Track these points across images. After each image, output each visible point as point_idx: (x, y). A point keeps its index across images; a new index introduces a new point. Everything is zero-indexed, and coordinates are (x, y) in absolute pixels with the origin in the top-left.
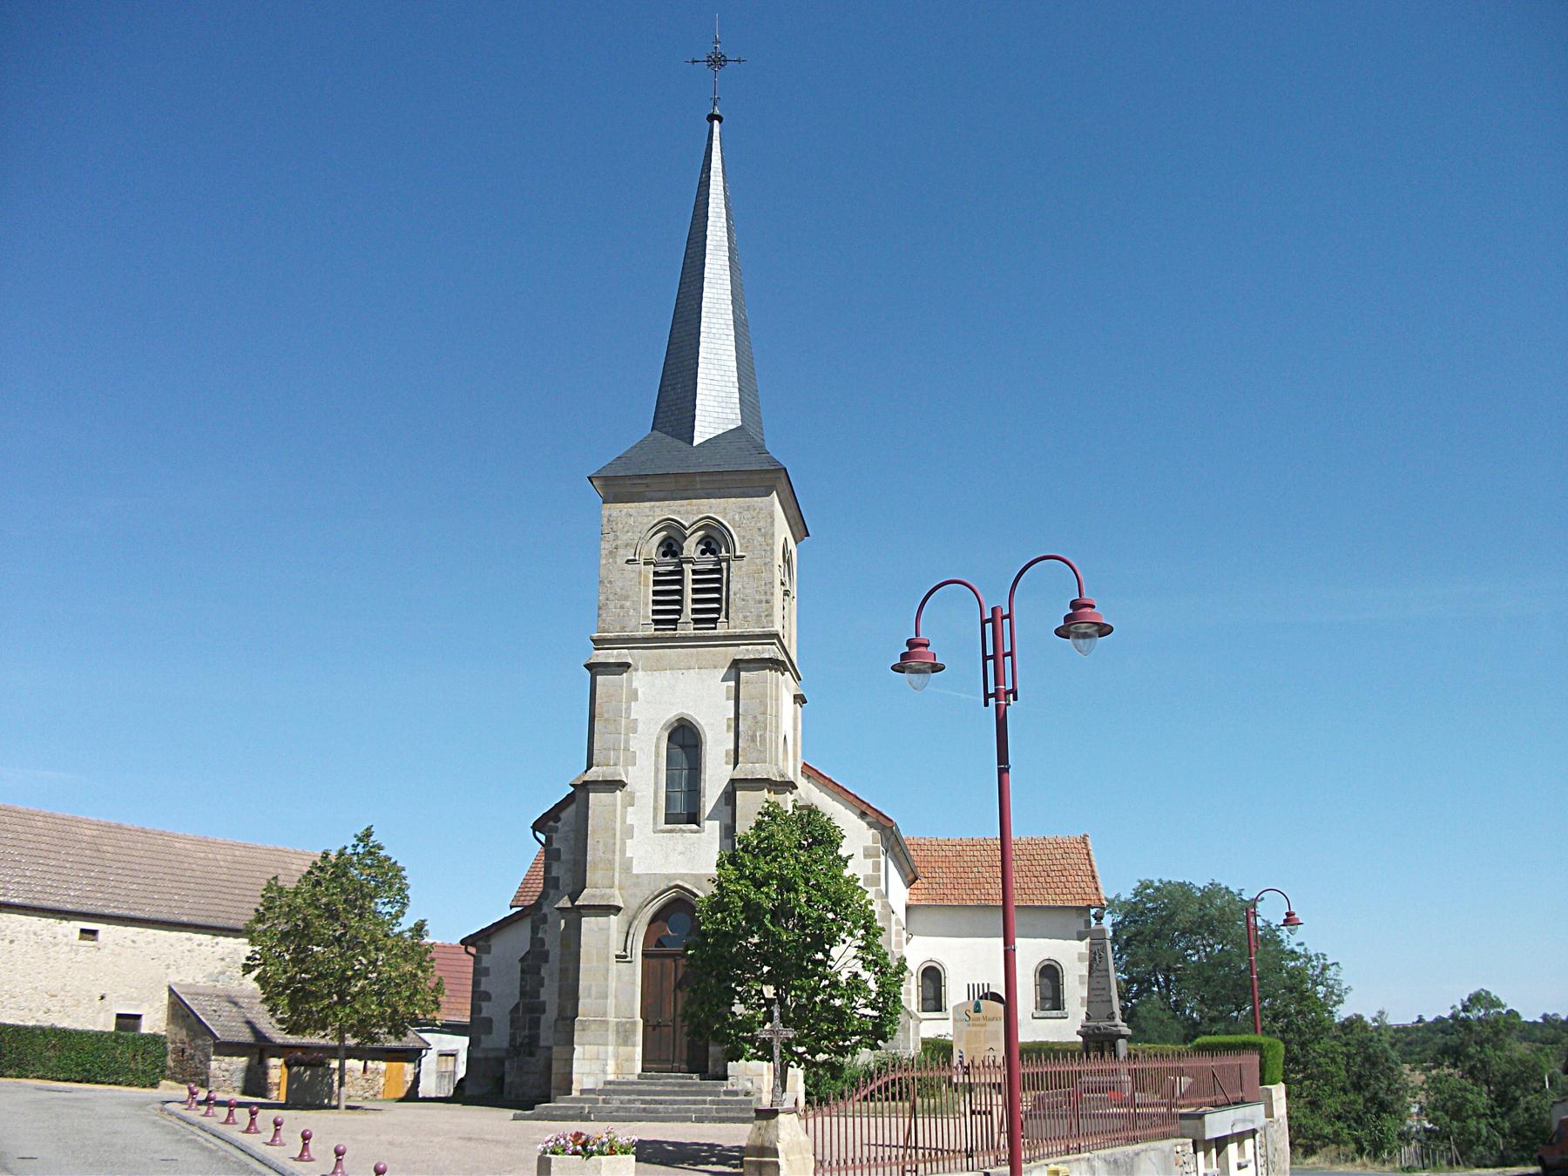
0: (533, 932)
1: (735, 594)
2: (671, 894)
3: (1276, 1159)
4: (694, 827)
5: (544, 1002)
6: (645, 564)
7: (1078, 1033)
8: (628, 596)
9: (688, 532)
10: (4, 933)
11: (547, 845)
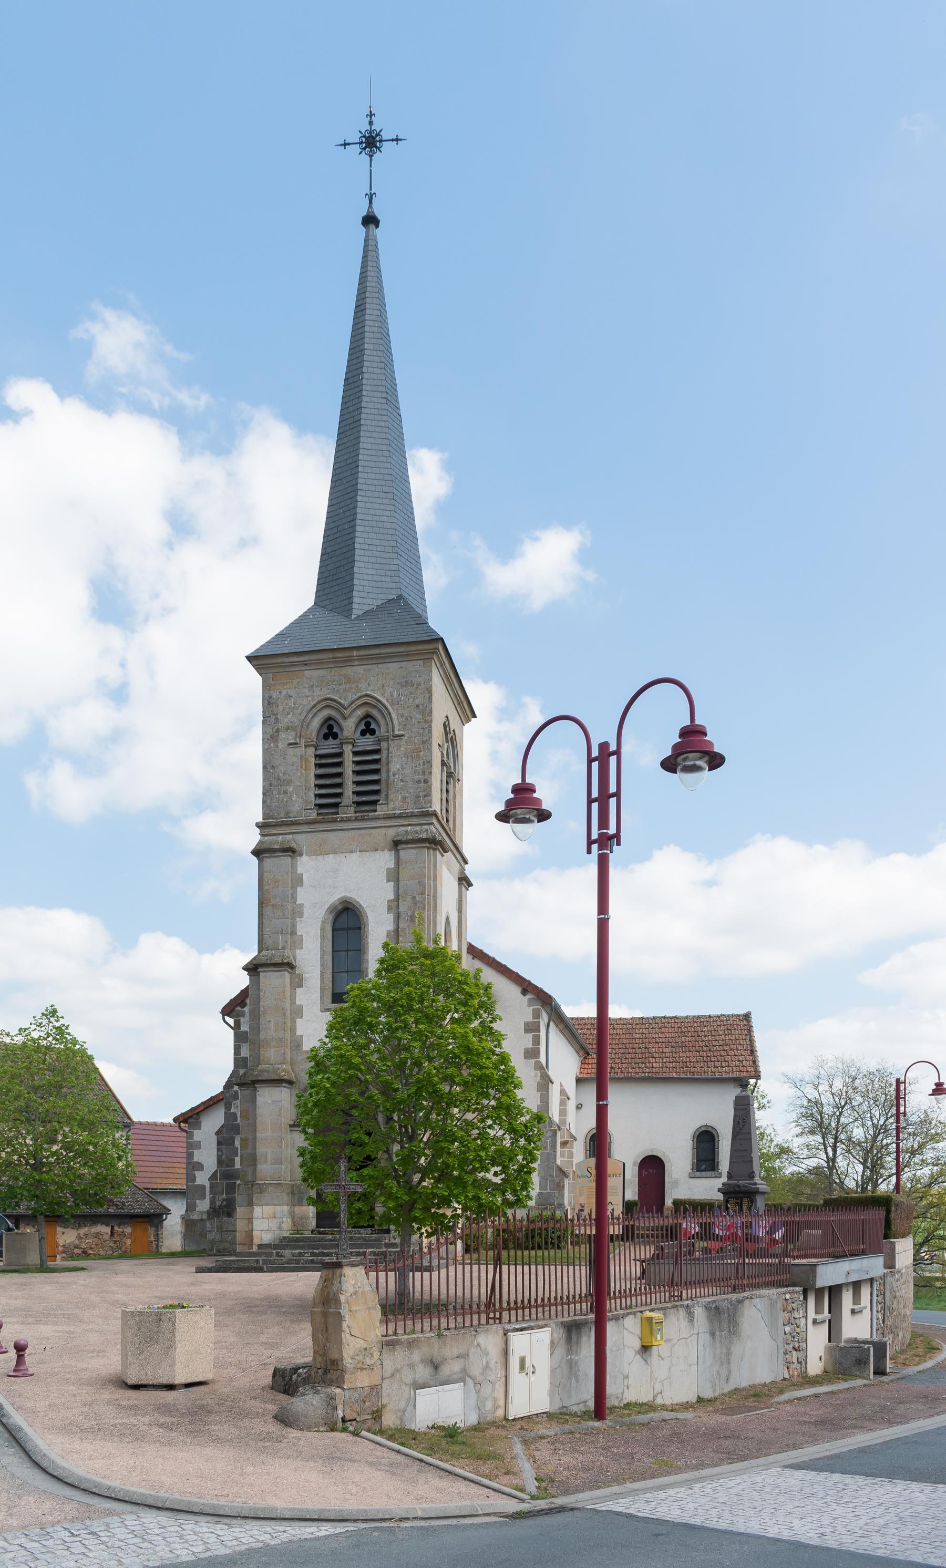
3: (895, 1306)
6: (306, 746)
7: (719, 1190)
8: (291, 781)
9: (347, 712)
11: (236, 1027)
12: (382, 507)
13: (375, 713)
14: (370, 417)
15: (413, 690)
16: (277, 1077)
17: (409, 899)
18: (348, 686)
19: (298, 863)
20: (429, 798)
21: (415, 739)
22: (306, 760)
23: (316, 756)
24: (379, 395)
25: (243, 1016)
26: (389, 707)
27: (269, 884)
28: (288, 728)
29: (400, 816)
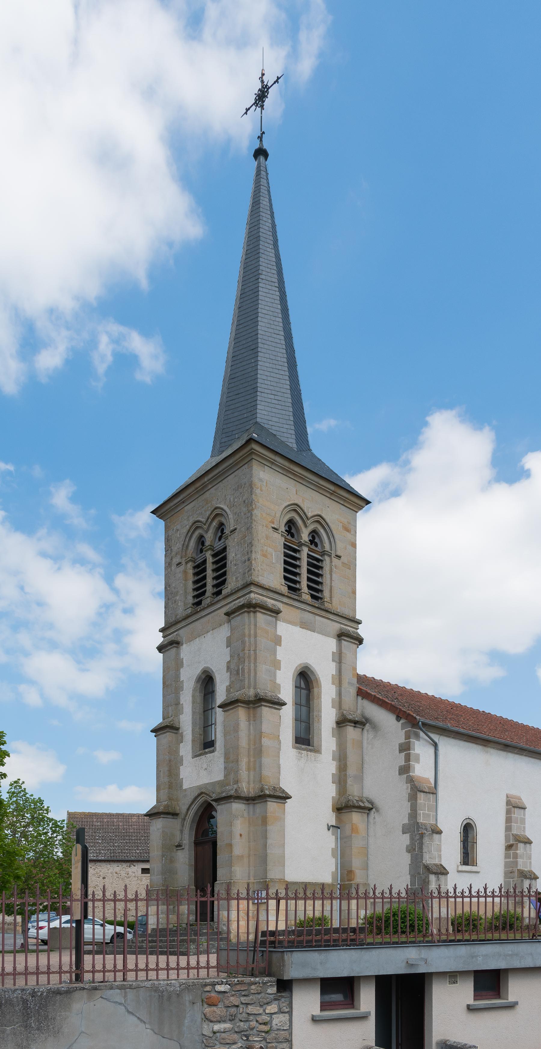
10: (99, 874)
13: (322, 531)
19: (181, 651)
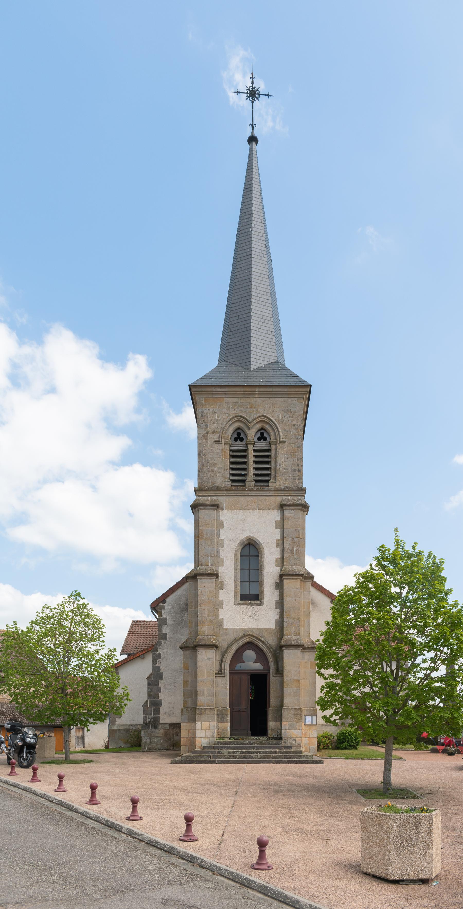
0: (153, 663)
1: (280, 465)
2: (245, 640)
4: (258, 602)
5: (161, 700)
6: (225, 444)
9: (251, 425)
12: (265, 307)
13: (267, 427)
14: (257, 254)
15: (291, 415)
16: (211, 644)
17: (290, 539)
18: (251, 409)
19: (221, 514)
20: (301, 481)
21: (293, 445)
22: (225, 452)
23: (231, 450)
24: (261, 242)
25: (164, 609)
26: (277, 424)
27: (203, 526)
28: (214, 432)
29: (284, 490)
